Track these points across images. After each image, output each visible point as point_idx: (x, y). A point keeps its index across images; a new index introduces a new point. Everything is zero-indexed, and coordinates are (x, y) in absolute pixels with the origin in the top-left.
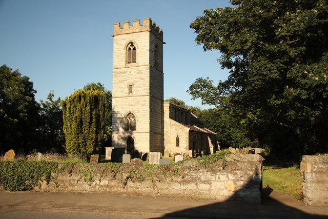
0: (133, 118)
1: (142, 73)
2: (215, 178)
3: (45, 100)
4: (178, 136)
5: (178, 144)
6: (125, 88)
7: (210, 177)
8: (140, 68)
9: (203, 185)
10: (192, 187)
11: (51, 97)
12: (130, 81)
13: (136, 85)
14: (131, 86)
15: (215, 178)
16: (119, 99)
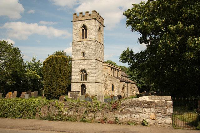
0: (85, 73)
1: (90, 45)
2: (143, 111)
3: (30, 61)
4: (113, 84)
5: (113, 90)
6: (80, 54)
7: (139, 110)
8: (89, 42)
9: (134, 115)
10: (127, 116)
11: (140, 34)
12: (83, 50)
14: (84, 53)
15: (143, 111)
16: (76, 61)
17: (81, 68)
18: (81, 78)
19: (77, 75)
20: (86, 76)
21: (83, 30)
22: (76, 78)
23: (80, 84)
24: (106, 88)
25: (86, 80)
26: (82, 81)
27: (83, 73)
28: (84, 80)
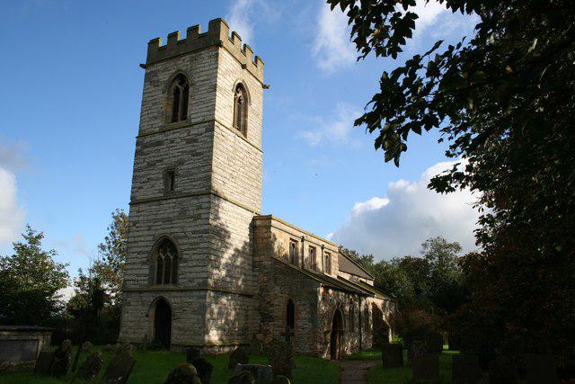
4: (290, 301)
6: (158, 179)
13: (181, 170)
14: (171, 175)
17: (159, 231)
18: (159, 274)
19: (143, 263)
20: (176, 266)
21: (177, 92)
22: (138, 272)
23: (149, 298)
24: (266, 317)
25: (175, 282)
26: (162, 286)
27: (164, 253)
28: (167, 282)
